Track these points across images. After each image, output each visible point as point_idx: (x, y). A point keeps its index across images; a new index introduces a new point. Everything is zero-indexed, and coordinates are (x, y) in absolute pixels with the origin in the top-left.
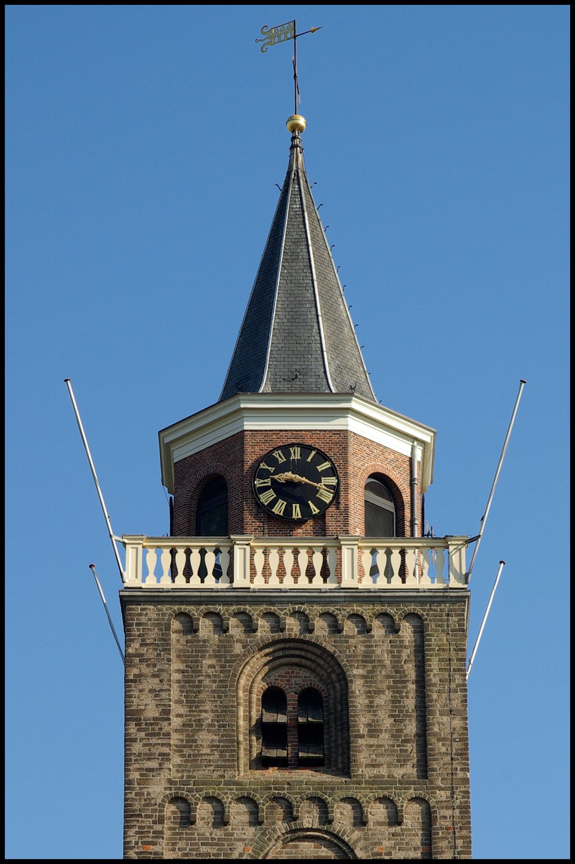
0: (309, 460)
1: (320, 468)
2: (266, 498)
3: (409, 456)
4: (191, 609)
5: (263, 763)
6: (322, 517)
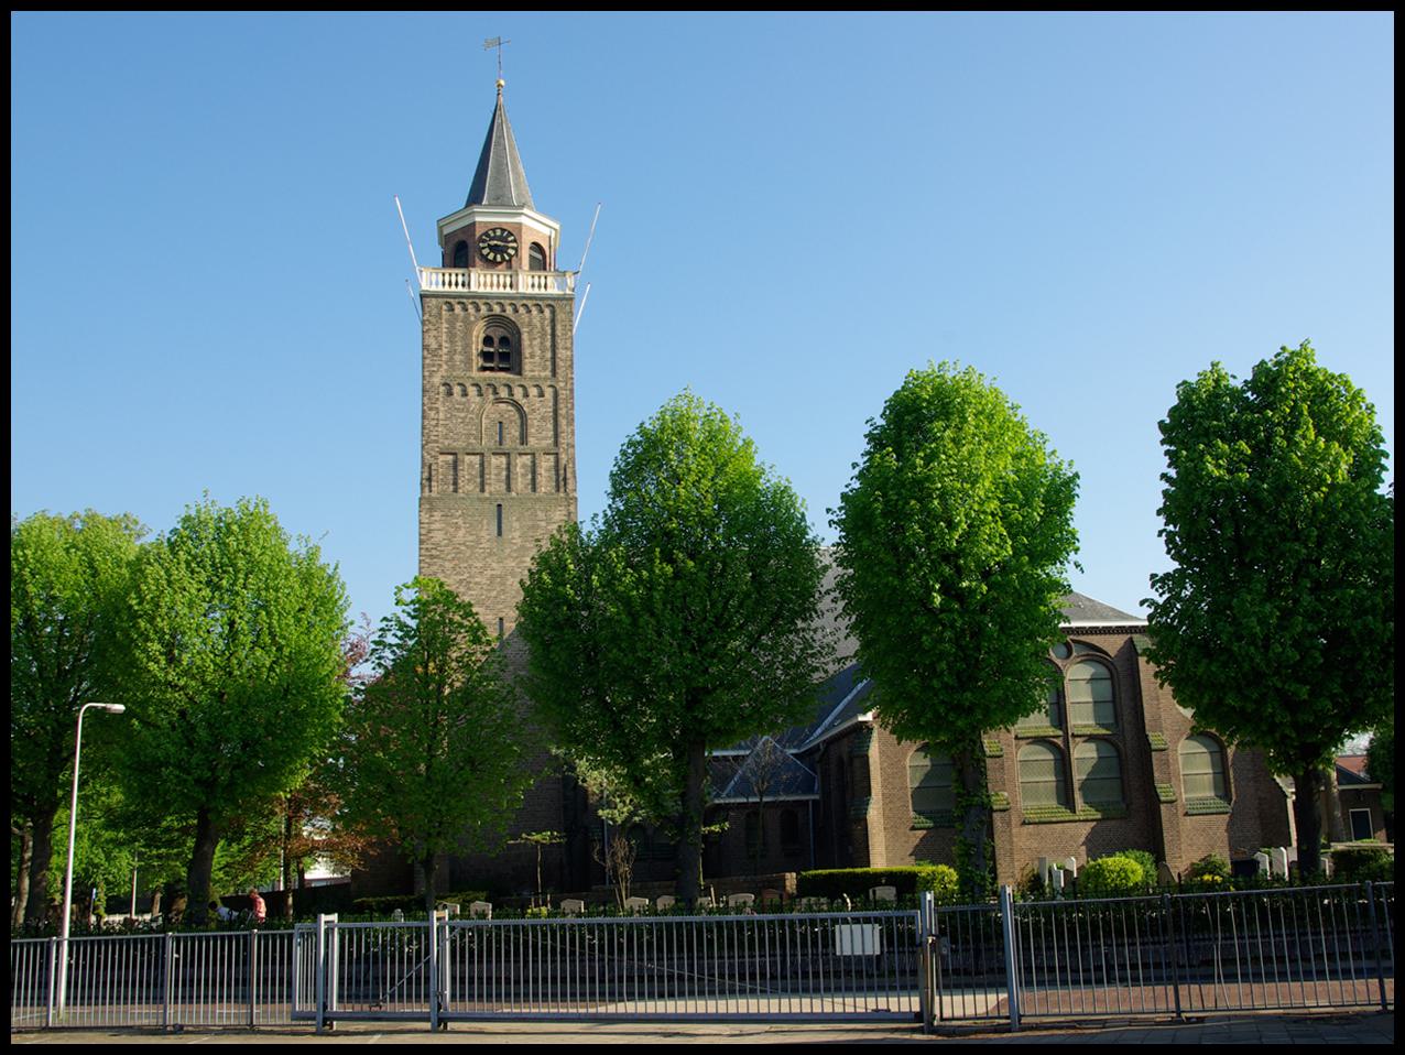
2: (485, 252)
5: (484, 369)
6: (510, 261)
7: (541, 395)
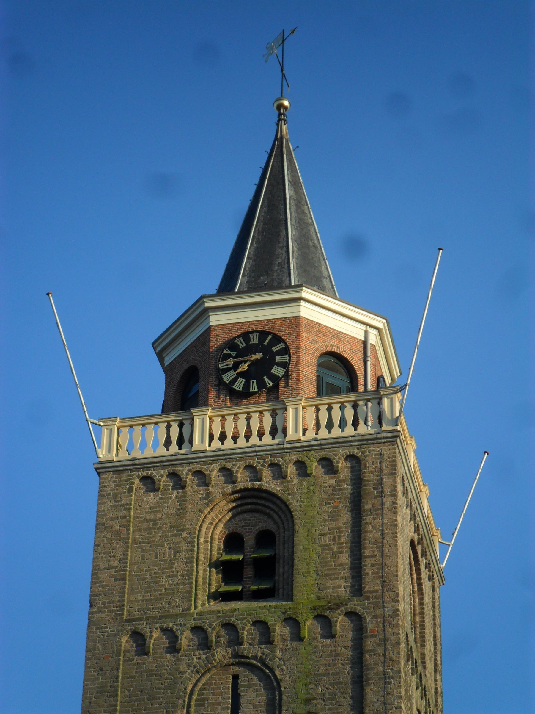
0: (265, 343)
1: (274, 349)
2: (227, 378)
3: (363, 339)
4: (153, 472)
6: (276, 387)
7: (329, 632)
